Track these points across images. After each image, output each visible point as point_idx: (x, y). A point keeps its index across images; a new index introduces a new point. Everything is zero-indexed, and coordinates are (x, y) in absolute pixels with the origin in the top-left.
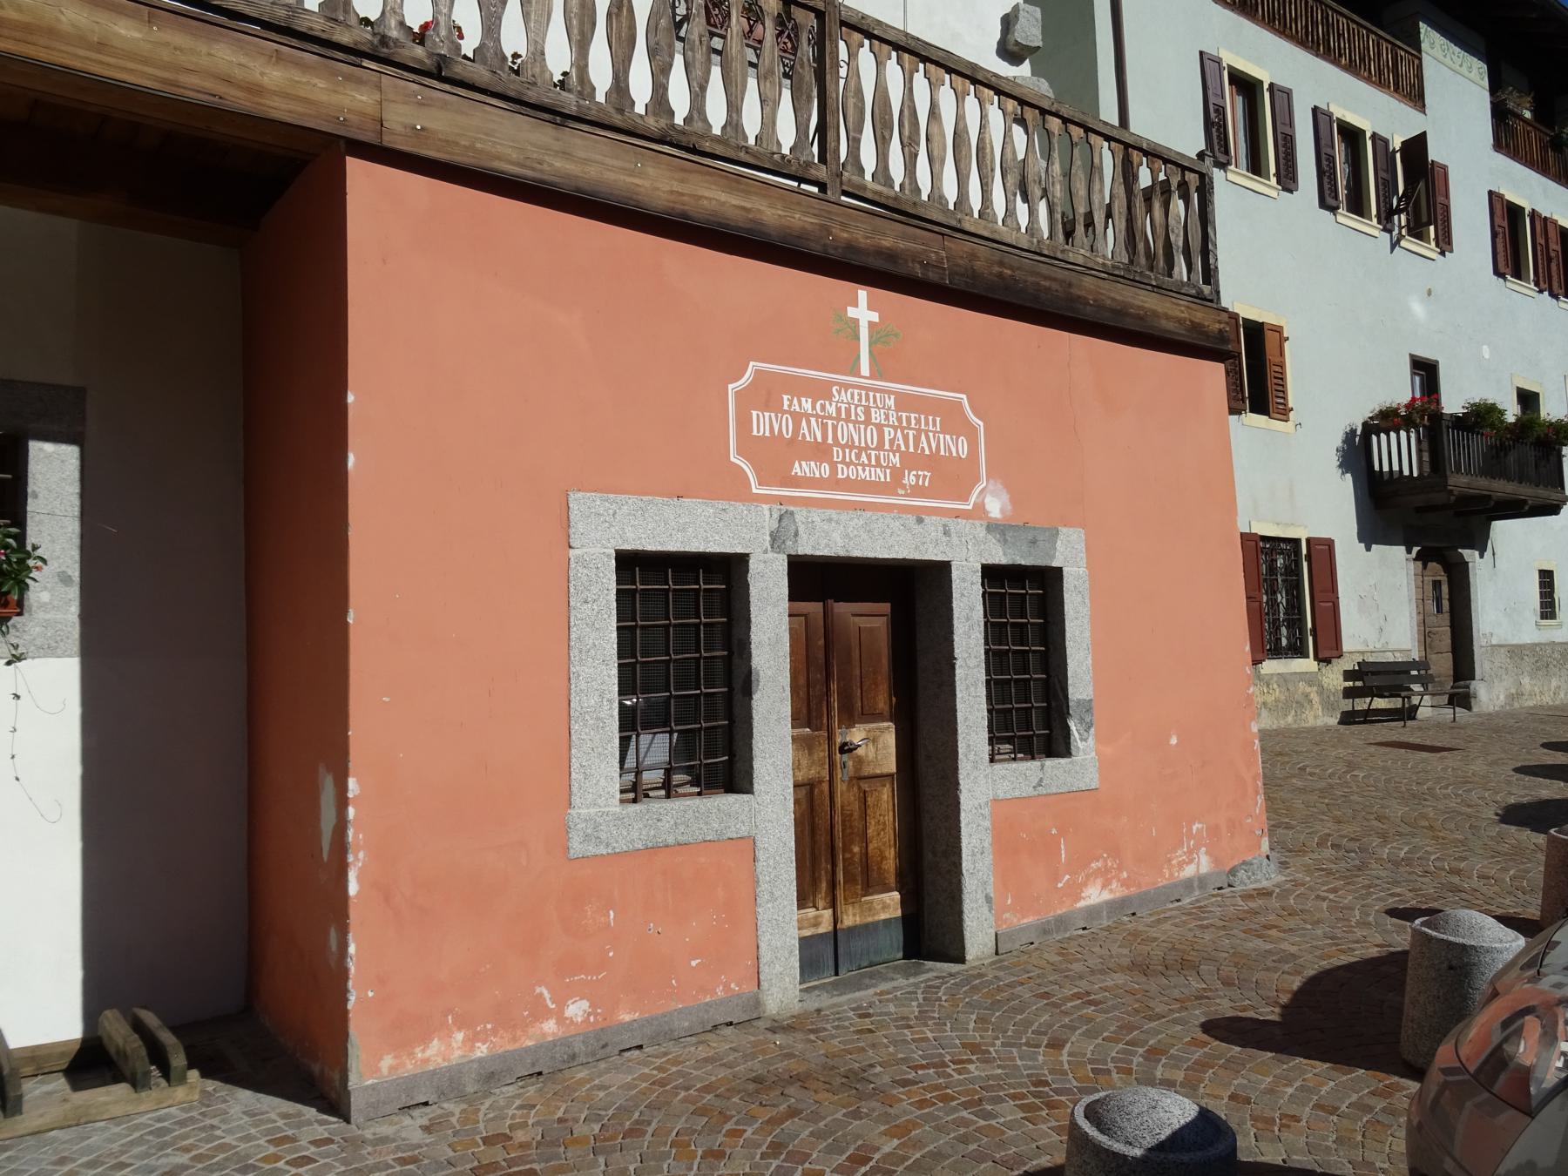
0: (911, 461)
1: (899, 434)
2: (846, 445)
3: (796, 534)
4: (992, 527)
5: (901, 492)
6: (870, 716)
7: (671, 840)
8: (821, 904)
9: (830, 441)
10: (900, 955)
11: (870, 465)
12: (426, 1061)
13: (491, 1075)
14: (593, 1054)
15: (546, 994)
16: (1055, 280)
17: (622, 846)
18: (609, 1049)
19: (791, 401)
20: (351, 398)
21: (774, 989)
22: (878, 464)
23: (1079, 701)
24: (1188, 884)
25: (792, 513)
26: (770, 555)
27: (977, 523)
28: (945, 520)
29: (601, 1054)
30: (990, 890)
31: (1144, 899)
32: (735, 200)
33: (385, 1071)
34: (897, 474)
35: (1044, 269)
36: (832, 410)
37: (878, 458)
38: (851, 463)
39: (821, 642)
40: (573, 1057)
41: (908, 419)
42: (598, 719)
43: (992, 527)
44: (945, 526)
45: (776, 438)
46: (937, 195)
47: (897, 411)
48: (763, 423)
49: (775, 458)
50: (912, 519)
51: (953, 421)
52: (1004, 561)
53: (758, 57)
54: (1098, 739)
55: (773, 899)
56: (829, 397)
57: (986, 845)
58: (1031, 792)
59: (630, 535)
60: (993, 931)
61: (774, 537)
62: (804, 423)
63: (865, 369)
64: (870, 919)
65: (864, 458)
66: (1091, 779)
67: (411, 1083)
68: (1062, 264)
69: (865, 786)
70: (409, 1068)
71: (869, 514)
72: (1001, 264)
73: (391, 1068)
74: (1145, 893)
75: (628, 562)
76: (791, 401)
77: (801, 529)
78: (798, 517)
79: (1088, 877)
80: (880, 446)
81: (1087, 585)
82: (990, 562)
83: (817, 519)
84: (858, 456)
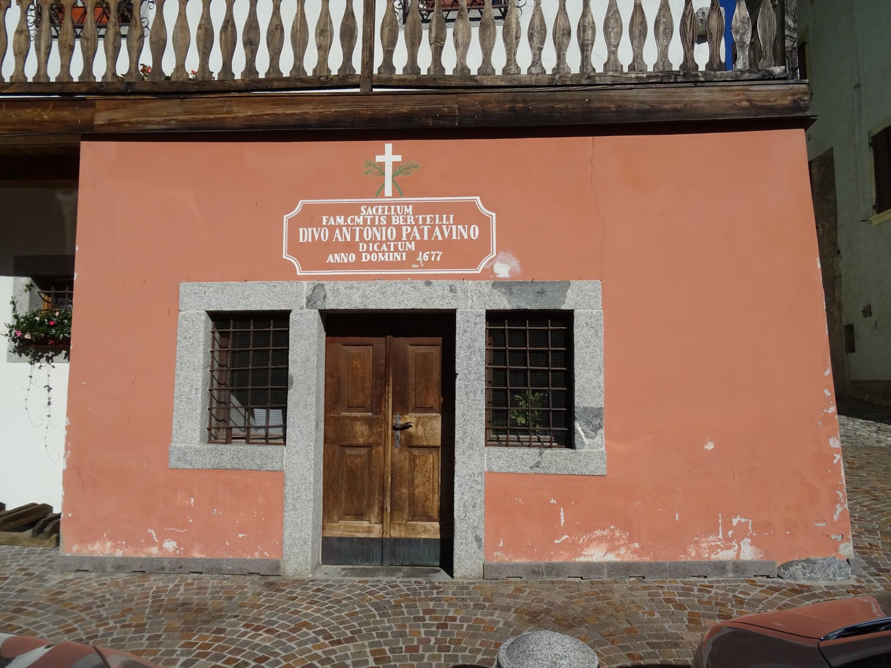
0: (422, 246)
1: (415, 229)
2: (371, 241)
3: (325, 297)
4: (498, 284)
5: (414, 266)
6: (425, 408)
7: (229, 466)
8: (373, 520)
9: (357, 239)
10: (438, 563)
11: (389, 251)
12: (93, 552)
13: (120, 566)
14: (174, 569)
15: (154, 534)
16: (572, 101)
17: (198, 465)
18: (182, 570)
19: (328, 220)
20: (77, 248)
21: (291, 562)
22: (396, 249)
23: (586, 409)
24: (720, 567)
25: (323, 285)
26: (305, 310)
27: (483, 282)
28: (450, 282)
29: (178, 570)
30: (481, 533)
31: (655, 569)
32: (268, 110)
33: (74, 551)
34: (412, 257)
35: (560, 96)
36: (360, 221)
37: (396, 247)
38: (374, 251)
39: (383, 362)
40: (163, 568)
41: (424, 220)
42: (189, 398)
43: (498, 284)
44: (451, 286)
45: (316, 243)
46: (462, 69)
47: (414, 215)
48: (306, 235)
49: (314, 256)
50: (421, 283)
51: (466, 215)
52: (508, 307)
53: (481, 13)
54: (608, 436)
55: (295, 509)
56: (358, 213)
57: (478, 501)
58: (527, 470)
59: (214, 303)
60: (481, 562)
61: (309, 300)
62: (337, 231)
63: (388, 190)
64: (413, 536)
65: (384, 247)
66: (599, 467)
67: (82, 560)
68: (580, 88)
69: (416, 452)
70: (85, 553)
71: (384, 282)
72: (515, 101)
73: (77, 551)
74: (659, 564)
75: (219, 318)
76: (328, 220)
77: (329, 294)
78: (327, 287)
79: (590, 541)
80: (399, 237)
81: (602, 322)
82: (495, 307)
83: (341, 287)
84: (379, 247)
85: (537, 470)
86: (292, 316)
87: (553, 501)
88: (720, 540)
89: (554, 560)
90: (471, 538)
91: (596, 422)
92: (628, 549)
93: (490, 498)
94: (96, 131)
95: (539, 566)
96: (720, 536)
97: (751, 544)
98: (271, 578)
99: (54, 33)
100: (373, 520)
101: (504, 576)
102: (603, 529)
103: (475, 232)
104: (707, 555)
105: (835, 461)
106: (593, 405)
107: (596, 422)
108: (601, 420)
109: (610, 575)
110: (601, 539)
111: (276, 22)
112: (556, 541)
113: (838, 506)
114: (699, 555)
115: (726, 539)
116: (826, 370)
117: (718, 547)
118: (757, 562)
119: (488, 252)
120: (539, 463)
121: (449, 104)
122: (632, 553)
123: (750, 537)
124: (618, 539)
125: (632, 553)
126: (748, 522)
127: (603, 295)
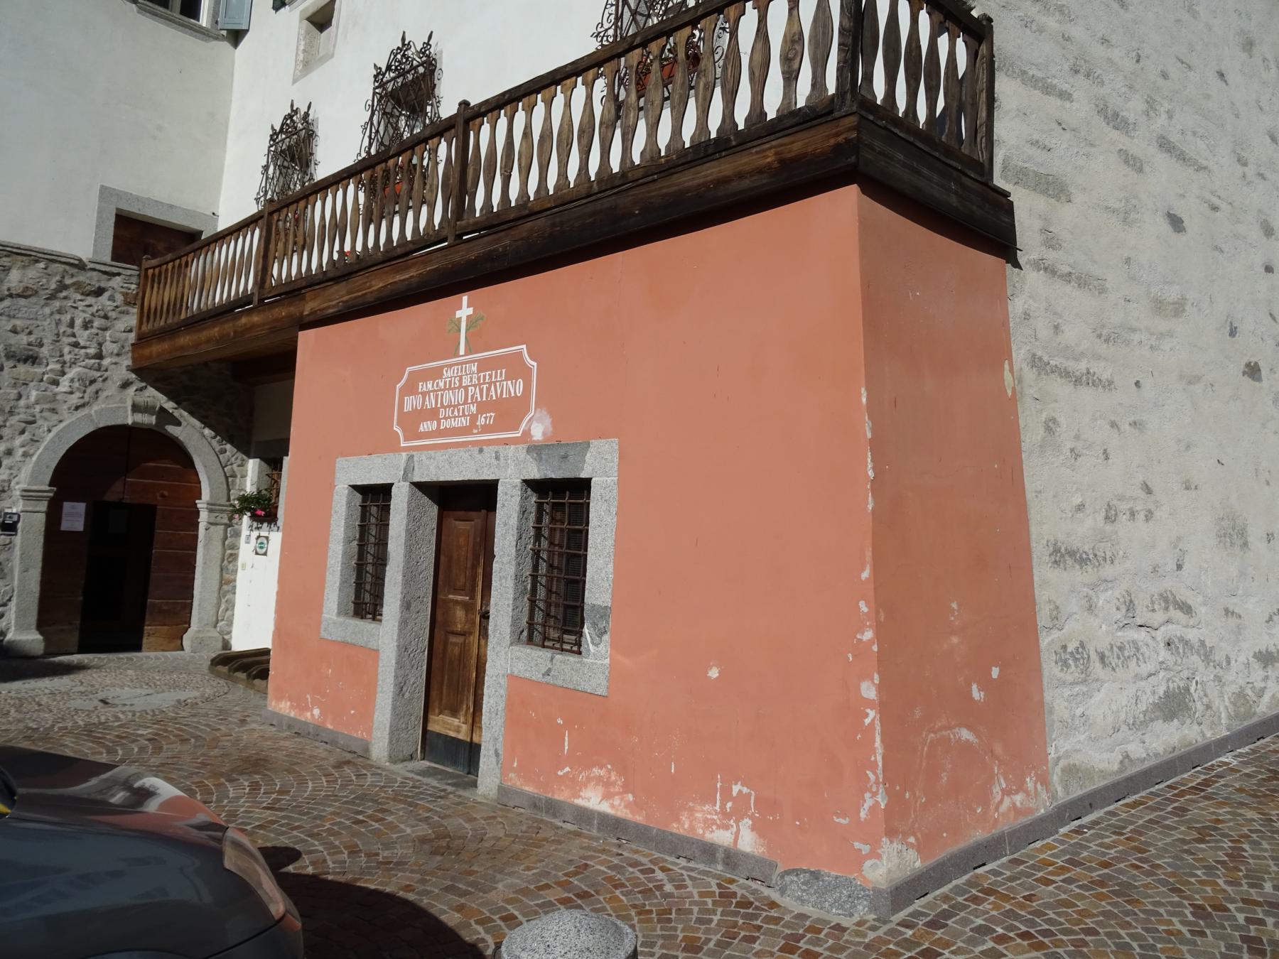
0: (483, 407)
24: (709, 851)
28: (496, 448)
51: (515, 368)
66: (599, 684)
79: (589, 779)
85: (547, 679)
86: (394, 490)
87: (560, 721)
88: (716, 813)
89: (556, 797)
90: (492, 752)
91: (602, 624)
92: (622, 799)
93: (510, 707)
94: (307, 320)
95: (540, 800)
96: (717, 808)
97: (753, 829)
98: (356, 757)
99: (666, 94)
100: (462, 719)
101: (511, 804)
102: (601, 767)
103: (517, 388)
104: (701, 832)
105: (867, 721)
106: (600, 603)
107: (602, 624)
108: (607, 622)
109: (599, 830)
110: (599, 780)
111: (795, 29)
112: (560, 773)
113: (867, 795)
114: (692, 828)
115: (725, 815)
116: (863, 570)
117: (714, 822)
118: (753, 857)
119: (528, 411)
120: (549, 670)
121: (504, 242)
122: (626, 807)
123: (752, 817)
124: (613, 784)
125: (626, 807)
126: (749, 794)
127: (621, 458)
